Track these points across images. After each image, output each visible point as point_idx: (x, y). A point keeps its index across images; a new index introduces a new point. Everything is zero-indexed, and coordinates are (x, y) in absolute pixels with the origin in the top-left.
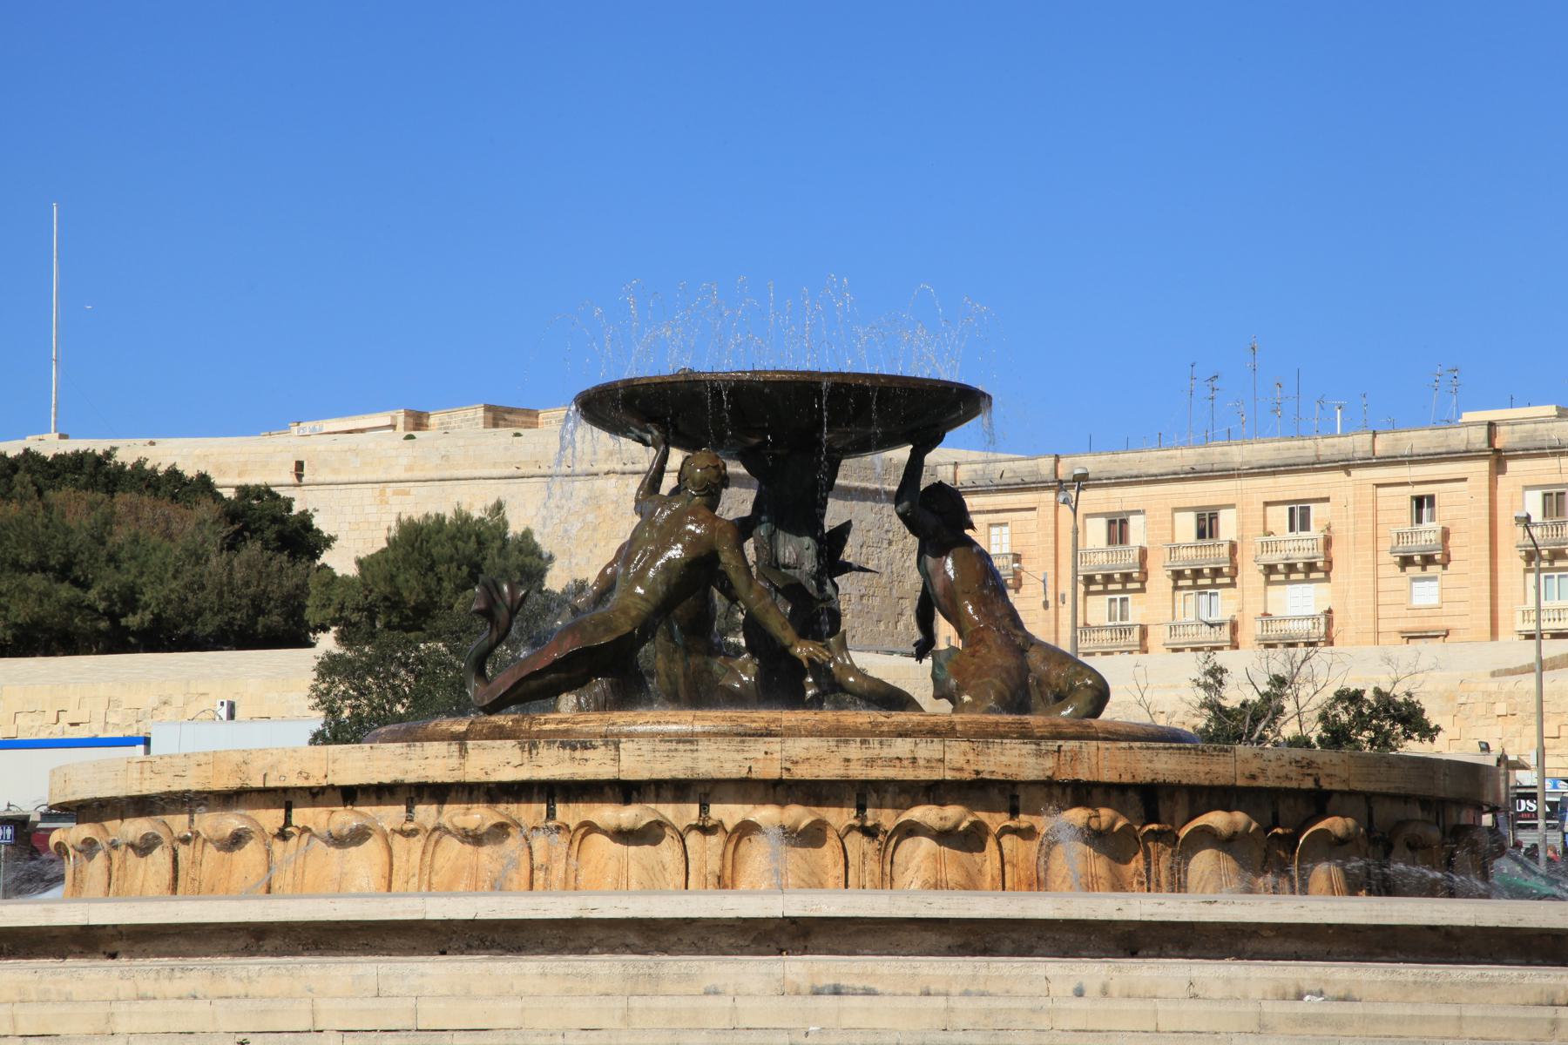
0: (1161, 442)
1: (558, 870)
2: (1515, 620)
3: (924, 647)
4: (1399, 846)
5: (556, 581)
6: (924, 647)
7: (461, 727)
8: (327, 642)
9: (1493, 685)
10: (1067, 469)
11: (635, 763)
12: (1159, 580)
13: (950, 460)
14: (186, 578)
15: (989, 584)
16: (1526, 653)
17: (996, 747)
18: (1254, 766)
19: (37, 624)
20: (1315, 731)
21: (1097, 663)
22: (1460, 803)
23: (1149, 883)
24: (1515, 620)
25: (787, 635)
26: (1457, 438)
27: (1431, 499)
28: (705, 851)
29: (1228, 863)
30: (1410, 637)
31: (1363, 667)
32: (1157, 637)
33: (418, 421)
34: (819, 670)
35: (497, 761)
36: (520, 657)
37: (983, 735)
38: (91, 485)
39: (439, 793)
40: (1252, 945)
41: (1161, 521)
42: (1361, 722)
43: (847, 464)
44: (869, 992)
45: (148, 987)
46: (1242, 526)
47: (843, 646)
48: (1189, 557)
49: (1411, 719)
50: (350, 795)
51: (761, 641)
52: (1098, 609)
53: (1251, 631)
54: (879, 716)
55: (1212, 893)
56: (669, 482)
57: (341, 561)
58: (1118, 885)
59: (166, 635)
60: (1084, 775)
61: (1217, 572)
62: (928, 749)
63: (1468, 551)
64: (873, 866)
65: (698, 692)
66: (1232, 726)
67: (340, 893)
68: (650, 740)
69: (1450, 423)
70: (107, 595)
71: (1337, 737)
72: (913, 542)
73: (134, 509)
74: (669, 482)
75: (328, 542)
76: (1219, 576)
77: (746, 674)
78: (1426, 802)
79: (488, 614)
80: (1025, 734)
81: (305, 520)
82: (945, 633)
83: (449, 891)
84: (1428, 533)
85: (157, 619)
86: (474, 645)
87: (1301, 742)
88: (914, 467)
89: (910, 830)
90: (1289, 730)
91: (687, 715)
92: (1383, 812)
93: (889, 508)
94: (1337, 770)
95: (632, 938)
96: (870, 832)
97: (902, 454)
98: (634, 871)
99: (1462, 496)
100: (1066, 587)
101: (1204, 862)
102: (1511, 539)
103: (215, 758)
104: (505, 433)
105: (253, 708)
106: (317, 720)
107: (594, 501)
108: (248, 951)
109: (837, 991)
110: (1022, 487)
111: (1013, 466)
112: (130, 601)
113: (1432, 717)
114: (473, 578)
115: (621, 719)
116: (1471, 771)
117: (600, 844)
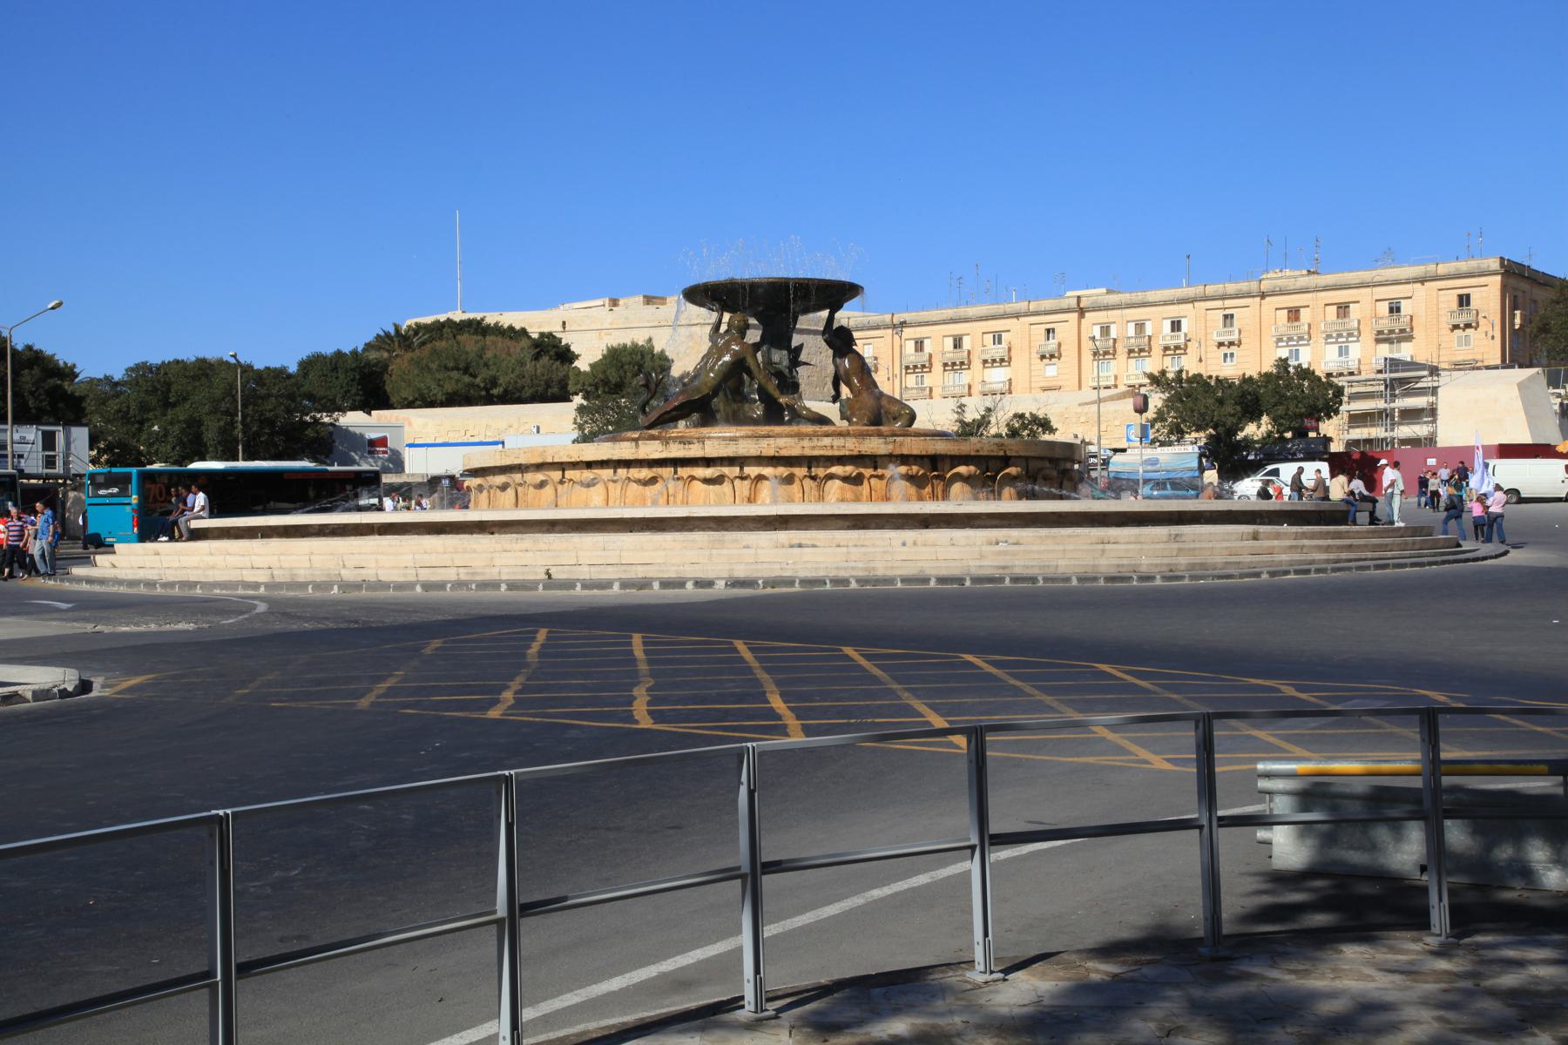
0: (937, 306)
1: (680, 497)
2: (1089, 381)
3: (836, 398)
4: (1040, 480)
5: (676, 372)
6: (836, 398)
7: (636, 435)
8: (578, 400)
9: (1079, 409)
10: (898, 319)
11: (711, 450)
12: (937, 367)
13: (845, 317)
14: (517, 372)
15: (864, 371)
16: (1094, 395)
17: (867, 441)
18: (978, 446)
19: (455, 393)
20: (1004, 431)
21: (911, 404)
22: (1065, 460)
23: (934, 497)
24: (1089, 381)
25: (776, 393)
26: (1064, 303)
27: (1468, 296)
28: (743, 487)
29: (967, 488)
30: (1045, 389)
31: (1026, 403)
32: (936, 392)
33: (614, 303)
34: (791, 408)
35: (652, 450)
36: (658, 406)
37: (862, 435)
38: (476, 333)
39: (627, 464)
40: (977, 522)
41: (938, 342)
42: (1024, 427)
43: (801, 318)
44: (814, 546)
45: (508, 546)
46: (973, 343)
47: (800, 397)
48: (950, 353)
49: (1046, 425)
50: (589, 465)
51: (767, 399)
52: (911, 380)
53: (976, 389)
54: (817, 428)
55: (960, 501)
56: (723, 328)
57: (583, 365)
58: (920, 498)
59: (510, 397)
60: (905, 452)
61: (962, 363)
62: (838, 442)
63: (1069, 352)
64: (814, 492)
65: (736, 419)
66: (969, 430)
67: (586, 506)
68: (719, 440)
69: (1061, 296)
70: (484, 380)
71: (1014, 433)
72: (831, 352)
73: (494, 343)
74: (723, 328)
75: (577, 357)
76: (964, 365)
77: (759, 412)
78: (1051, 460)
79: (646, 386)
80: (880, 435)
81: (567, 347)
82: (845, 392)
83: (633, 505)
84: (1052, 345)
85: (506, 391)
86: (644, 397)
87: (998, 436)
88: (831, 319)
89: (831, 477)
90: (993, 431)
91: (733, 429)
92: (1034, 465)
93: (820, 338)
94: (1013, 447)
95: (712, 525)
96: (813, 478)
97: (825, 313)
98: (712, 496)
99: (1066, 327)
100: (897, 371)
101: (957, 487)
102: (1087, 346)
103: (532, 450)
104: (652, 308)
105: (549, 428)
106: (576, 434)
107: (691, 336)
108: (549, 531)
109: (800, 546)
110: (877, 328)
111: (875, 318)
112: (494, 382)
113: (1054, 424)
114: (640, 371)
115: (705, 431)
116: (1070, 447)
117: (697, 485)
